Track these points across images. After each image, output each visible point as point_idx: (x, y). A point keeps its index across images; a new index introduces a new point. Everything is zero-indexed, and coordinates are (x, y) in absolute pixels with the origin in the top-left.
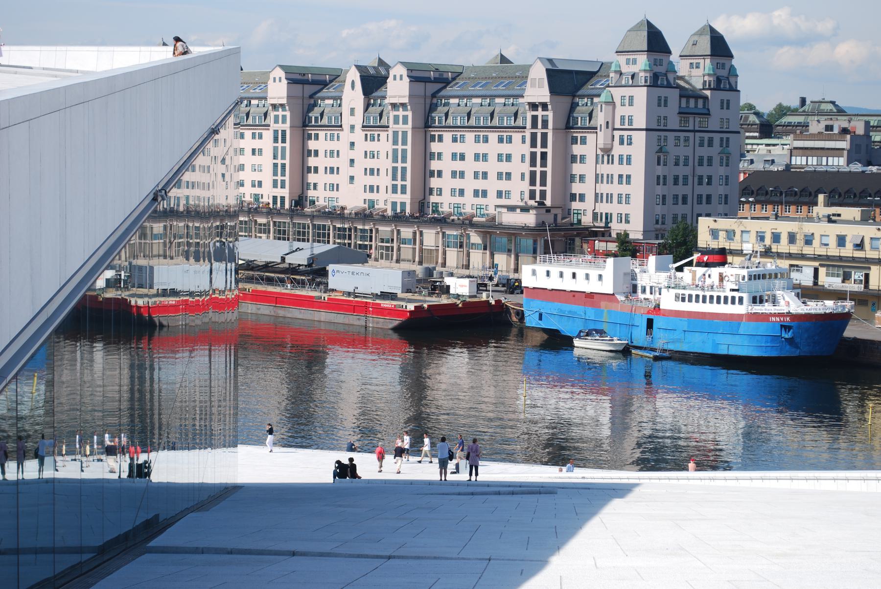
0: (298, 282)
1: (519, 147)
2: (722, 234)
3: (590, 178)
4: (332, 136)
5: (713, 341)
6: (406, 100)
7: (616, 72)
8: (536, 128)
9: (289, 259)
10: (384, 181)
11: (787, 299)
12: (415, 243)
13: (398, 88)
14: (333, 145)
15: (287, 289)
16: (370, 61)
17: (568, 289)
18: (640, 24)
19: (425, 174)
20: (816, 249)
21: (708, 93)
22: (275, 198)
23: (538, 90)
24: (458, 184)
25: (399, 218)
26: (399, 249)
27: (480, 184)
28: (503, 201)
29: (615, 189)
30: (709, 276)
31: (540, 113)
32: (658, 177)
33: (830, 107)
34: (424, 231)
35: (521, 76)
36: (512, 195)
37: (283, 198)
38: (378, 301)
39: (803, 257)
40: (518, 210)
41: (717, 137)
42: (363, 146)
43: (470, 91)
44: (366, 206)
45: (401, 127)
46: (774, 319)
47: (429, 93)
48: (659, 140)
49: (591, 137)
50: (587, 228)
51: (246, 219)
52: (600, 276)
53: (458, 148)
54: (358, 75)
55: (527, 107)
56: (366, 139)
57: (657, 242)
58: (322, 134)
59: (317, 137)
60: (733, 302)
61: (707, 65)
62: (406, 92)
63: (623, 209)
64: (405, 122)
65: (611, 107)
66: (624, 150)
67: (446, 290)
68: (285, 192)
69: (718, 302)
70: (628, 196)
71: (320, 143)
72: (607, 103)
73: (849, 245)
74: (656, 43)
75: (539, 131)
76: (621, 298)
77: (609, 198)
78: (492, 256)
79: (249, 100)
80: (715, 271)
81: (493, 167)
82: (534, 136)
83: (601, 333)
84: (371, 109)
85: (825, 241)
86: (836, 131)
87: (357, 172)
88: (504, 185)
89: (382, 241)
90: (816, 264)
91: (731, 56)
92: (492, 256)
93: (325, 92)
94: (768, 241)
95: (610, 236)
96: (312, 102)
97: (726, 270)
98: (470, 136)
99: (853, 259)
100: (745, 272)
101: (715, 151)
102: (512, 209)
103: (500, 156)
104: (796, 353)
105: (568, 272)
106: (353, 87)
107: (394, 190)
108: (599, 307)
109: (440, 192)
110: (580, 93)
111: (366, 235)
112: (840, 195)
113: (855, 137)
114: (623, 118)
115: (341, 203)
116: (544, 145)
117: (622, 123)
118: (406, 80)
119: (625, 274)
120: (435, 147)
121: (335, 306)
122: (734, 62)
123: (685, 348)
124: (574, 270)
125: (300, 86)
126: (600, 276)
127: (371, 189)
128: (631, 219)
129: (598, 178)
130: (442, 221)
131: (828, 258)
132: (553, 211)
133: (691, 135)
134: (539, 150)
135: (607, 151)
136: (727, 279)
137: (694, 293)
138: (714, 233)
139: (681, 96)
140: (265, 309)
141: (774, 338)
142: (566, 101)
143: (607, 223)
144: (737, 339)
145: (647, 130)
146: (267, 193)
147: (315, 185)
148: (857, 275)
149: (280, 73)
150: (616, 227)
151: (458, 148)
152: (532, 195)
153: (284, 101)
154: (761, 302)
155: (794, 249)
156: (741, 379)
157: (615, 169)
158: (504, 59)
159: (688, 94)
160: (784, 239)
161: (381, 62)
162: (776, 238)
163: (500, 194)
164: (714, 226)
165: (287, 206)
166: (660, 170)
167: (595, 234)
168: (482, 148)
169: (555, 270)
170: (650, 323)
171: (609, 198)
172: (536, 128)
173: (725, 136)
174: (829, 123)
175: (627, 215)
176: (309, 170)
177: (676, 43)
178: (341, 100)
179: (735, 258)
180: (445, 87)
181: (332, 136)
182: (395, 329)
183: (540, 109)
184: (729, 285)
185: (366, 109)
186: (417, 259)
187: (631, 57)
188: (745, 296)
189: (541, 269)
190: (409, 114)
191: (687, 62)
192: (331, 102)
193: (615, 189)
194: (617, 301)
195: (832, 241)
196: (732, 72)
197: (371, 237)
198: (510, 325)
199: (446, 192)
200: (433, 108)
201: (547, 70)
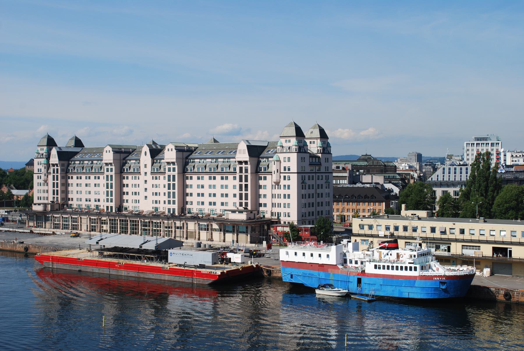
0: (149, 258)
1: (232, 182)
2: (366, 228)
3: (269, 196)
4: (135, 177)
5: (399, 290)
6: (174, 160)
7: (280, 146)
8: (242, 172)
9: (144, 247)
11: (437, 266)
12: (183, 228)
14: (136, 182)
15: (145, 263)
17: (308, 262)
18: (291, 124)
19: (184, 195)
21: (320, 155)
22: (107, 207)
23: (243, 155)
24: (201, 199)
25: (172, 217)
26: (175, 231)
27: (212, 199)
28: (225, 207)
29: (282, 201)
30: (391, 255)
31: (244, 166)
32: (303, 195)
34: (188, 223)
35: (233, 149)
36: (229, 204)
37: (112, 207)
38: (198, 270)
40: (237, 212)
41: (324, 175)
42: (151, 182)
43: (205, 156)
44: (154, 210)
46: (436, 279)
47: (184, 157)
48: (302, 177)
49: (269, 177)
51: (96, 218)
52: (328, 256)
53: (200, 182)
54: (148, 149)
55: (237, 163)
56: (153, 179)
58: (130, 177)
59: (127, 178)
61: (318, 142)
62: (175, 157)
63: (287, 210)
65: (279, 163)
66: (287, 182)
67: (229, 261)
68: (113, 204)
69: (397, 269)
70: (289, 204)
71: (129, 181)
72: (277, 161)
75: (243, 175)
76: (340, 267)
77: (279, 205)
78: (224, 234)
79: (92, 161)
80: (394, 252)
81: (218, 191)
82: (241, 177)
83: (331, 286)
84: (154, 164)
85: (424, 229)
86: (341, 169)
87: (149, 194)
88: (224, 200)
89: (166, 227)
91: (328, 138)
92: (224, 234)
93: (130, 157)
94: (392, 230)
95: (280, 223)
96: (124, 161)
98: (206, 177)
99: (441, 239)
101: (323, 182)
103: (95, 185)
104: (447, 296)
105: (308, 254)
106: (146, 154)
108: (328, 272)
109: (192, 203)
110: (261, 156)
111: (157, 225)
112: (356, 198)
113: (350, 171)
115: (141, 209)
118: (112, 153)
119: (341, 254)
120: (188, 182)
121: (172, 272)
122: (329, 141)
123: (382, 294)
124: (304, 252)
125: (119, 154)
126: (328, 256)
127: (156, 202)
128: (291, 215)
129: (273, 196)
130: (195, 218)
131: (427, 238)
132: (254, 212)
133: (314, 174)
134: (172, 182)
135: (278, 183)
136: (401, 256)
137: (386, 265)
138: (362, 227)
139: (310, 157)
140: (132, 273)
142: (256, 159)
143: (278, 217)
144: (414, 290)
145: (297, 173)
147: (127, 201)
148: (443, 247)
149: (109, 148)
151: (200, 182)
152: (241, 204)
153: (112, 162)
155: (407, 234)
156: (418, 310)
157: (282, 192)
158: (215, 141)
159: (313, 156)
160: (401, 229)
162: (396, 228)
163: (222, 204)
164: (362, 223)
165: (114, 211)
166: (303, 192)
168: (212, 182)
170: (359, 281)
171: (279, 205)
172: (242, 172)
173: (327, 174)
174: (337, 165)
175: (288, 213)
176: (124, 193)
178: (139, 160)
179: (374, 239)
180: (191, 154)
181: (135, 177)
182: (210, 285)
183: (244, 164)
185: (152, 165)
186: (185, 236)
187: (288, 139)
188: (418, 266)
192: (134, 161)
193: (282, 201)
194: (339, 269)
195: (428, 230)
196: (328, 145)
197: (160, 226)
198: (263, 277)
199: (195, 203)
200: (187, 164)
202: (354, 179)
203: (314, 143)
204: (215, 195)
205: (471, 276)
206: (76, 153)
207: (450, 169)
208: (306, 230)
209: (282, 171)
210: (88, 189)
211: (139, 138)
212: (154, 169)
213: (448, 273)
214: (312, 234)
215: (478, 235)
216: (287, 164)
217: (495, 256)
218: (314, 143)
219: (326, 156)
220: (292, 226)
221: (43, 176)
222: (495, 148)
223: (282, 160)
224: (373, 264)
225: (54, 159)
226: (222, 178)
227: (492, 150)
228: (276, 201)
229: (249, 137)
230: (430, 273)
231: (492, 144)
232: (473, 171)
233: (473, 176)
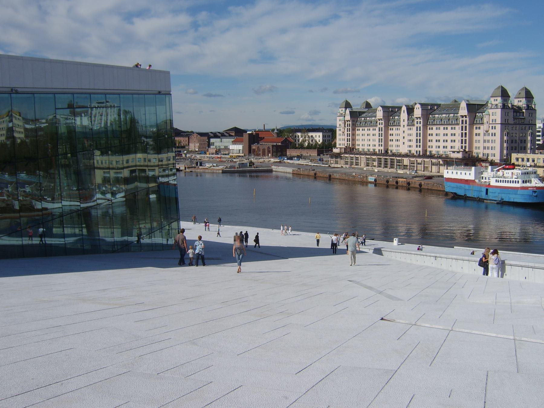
1: (458, 130)
2: (520, 160)
6: (420, 116)
10: (414, 143)
13: (418, 112)
18: (499, 87)
19: (386, 141)
22: (417, 151)
23: (463, 111)
28: (453, 150)
37: (420, 151)
42: (407, 132)
43: (450, 112)
45: (419, 125)
58: (394, 128)
60: (515, 183)
63: (493, 152)
66: (493, 131)
74: (504, 94)
75: (464, 125)
81: (449, 138)
82: (462, 127)
87: (406, 141)
97: (515, 171)
100: (520, 172)
102: (454, 152)
103: (444, 134)
107: (417, 147)
114: (493, 120)
115: (400, 151)
116: (466, 130)
117: (493, 122)
118: (420, 109)
130: (431, 156)
134: (464, 132)
138: (517, 159)
139: (514, 112)
141: (530, 196)
146: (377, 149)
149: (380, 108)
150: (490, 158)
152: (462, 147)
154: (526, 182)
157: (490, 138)
158: (455, 101)
164: (517, 157)
168: (445, 132)
169: (463, 172)
184: (514, 177)
185: (408, 120)
189: (450, 172)
191: (517, 100)
193: (490, 145)
201: (467, 104)
204: (447, 135)
206: (364, 112)
210: (369, 137)
211: (401, 101)
218: (521, 101)
221: (342, 128)
223: (491, 114)
225: (348, 117)
228: (486, 145)
230: (528, 185)
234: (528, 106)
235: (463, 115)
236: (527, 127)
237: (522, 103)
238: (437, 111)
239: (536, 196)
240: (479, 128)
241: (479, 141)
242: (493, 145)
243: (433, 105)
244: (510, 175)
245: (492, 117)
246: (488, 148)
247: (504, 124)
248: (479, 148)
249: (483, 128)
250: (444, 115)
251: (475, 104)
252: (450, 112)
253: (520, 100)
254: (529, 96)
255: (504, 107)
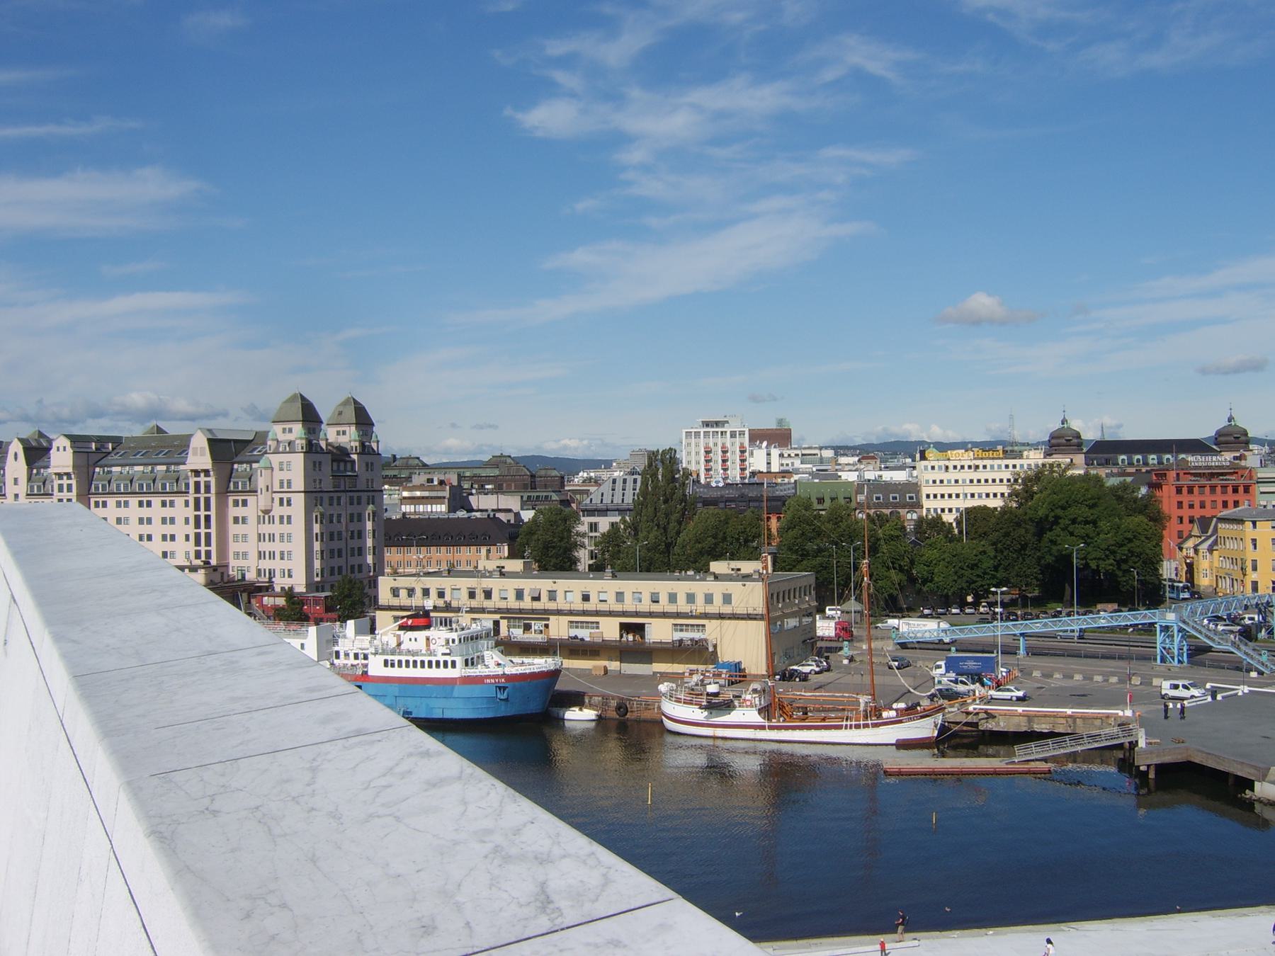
1: (182, 510)
2: (403, 593)
6: (70, 470)
13: (62, 458)
16: (28, 431)
18: (295, 395)
20: (496, 602)
23: (199, 457)
31: (202, 479)
33: (416, 462)
35: (181, 446)
36: (177, 555)
39: (483, 610)
43: (154, 459)
50: (252, 584)
53: (168, 512)
57: (324, 594)
63: (285, 565)
64: (70, 488)
66: (285, 511)
73: (527, 598)
74: (310, 416)
75: (202, 496)
80: (421, 635)
82: (197, 501)
86: (436, 483)
90: (497, 617)
99: (533, 611)
106: (16, 459)
113: (452, 487)
114: (282, 482)
117: (282, 486)
118: (70, 451)
128: (293, 574)
131: (508, 611)
138: (395, 592)
143: (270, 578)
148: (536, 625)
149: (61, 442)
150: (280, 583)
157: (276, 528)
161: (41, 435)
164: (395, 584)
167: (260, 589)
174: (429, 476)
177: (325, 412)
185: (29, 479)
190: (73, 482)
193: (277, 547)
195: (511, 596)
201: (209, 440)
202: (459, 500)
203: (344, 433)
205: (555, 674)
207: (625, 481)
208: (317, 601)
209: (277, 488)
212: (32, 488)
213: (510, 670)
214: (329, 609)
215: (597, 601)
216: (285, 475)
217: (624, 639)
218: (344, 433)
219: (369, 458)
220: (289, 594)
222: (738, 440)
223: (276, 466)
224: (381, 658)
226: (141, 504)
227: (715, 445)
228: (266, 547)
229: (212, 424)
230: (479, 671)
231: (733, 435)
232: (645, 483)
233: (644, 493)
234: (363, 445)
235: (199, 467)
236: (364, 496)
237: (348, 437)
238: (113, 458)
239: (506, 700)
240: (245, 503)
241: (245, 536)
242: (285, 547)
243: (102, 440)
244: (421, 645)
245: (278, 476)
246: (272, 555)
247: (313, 494)
248: (245, 555)
249: (262, 500)
250: (137, 468)
251: (229, 441)
252: (154, 459)
253: (341, 429)
254: (363, 420)
255: (311, 448)
